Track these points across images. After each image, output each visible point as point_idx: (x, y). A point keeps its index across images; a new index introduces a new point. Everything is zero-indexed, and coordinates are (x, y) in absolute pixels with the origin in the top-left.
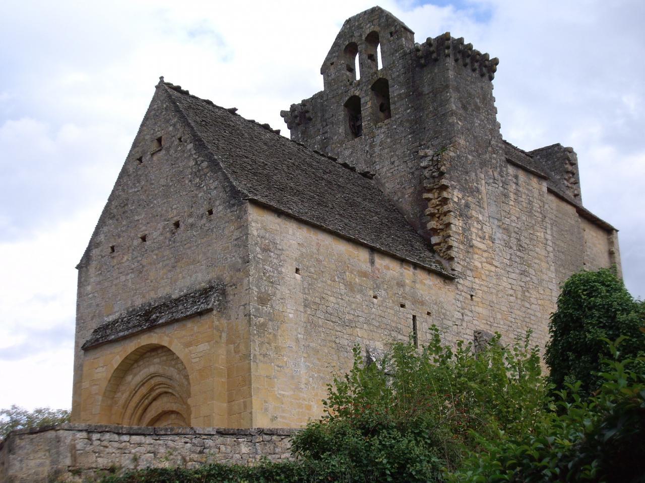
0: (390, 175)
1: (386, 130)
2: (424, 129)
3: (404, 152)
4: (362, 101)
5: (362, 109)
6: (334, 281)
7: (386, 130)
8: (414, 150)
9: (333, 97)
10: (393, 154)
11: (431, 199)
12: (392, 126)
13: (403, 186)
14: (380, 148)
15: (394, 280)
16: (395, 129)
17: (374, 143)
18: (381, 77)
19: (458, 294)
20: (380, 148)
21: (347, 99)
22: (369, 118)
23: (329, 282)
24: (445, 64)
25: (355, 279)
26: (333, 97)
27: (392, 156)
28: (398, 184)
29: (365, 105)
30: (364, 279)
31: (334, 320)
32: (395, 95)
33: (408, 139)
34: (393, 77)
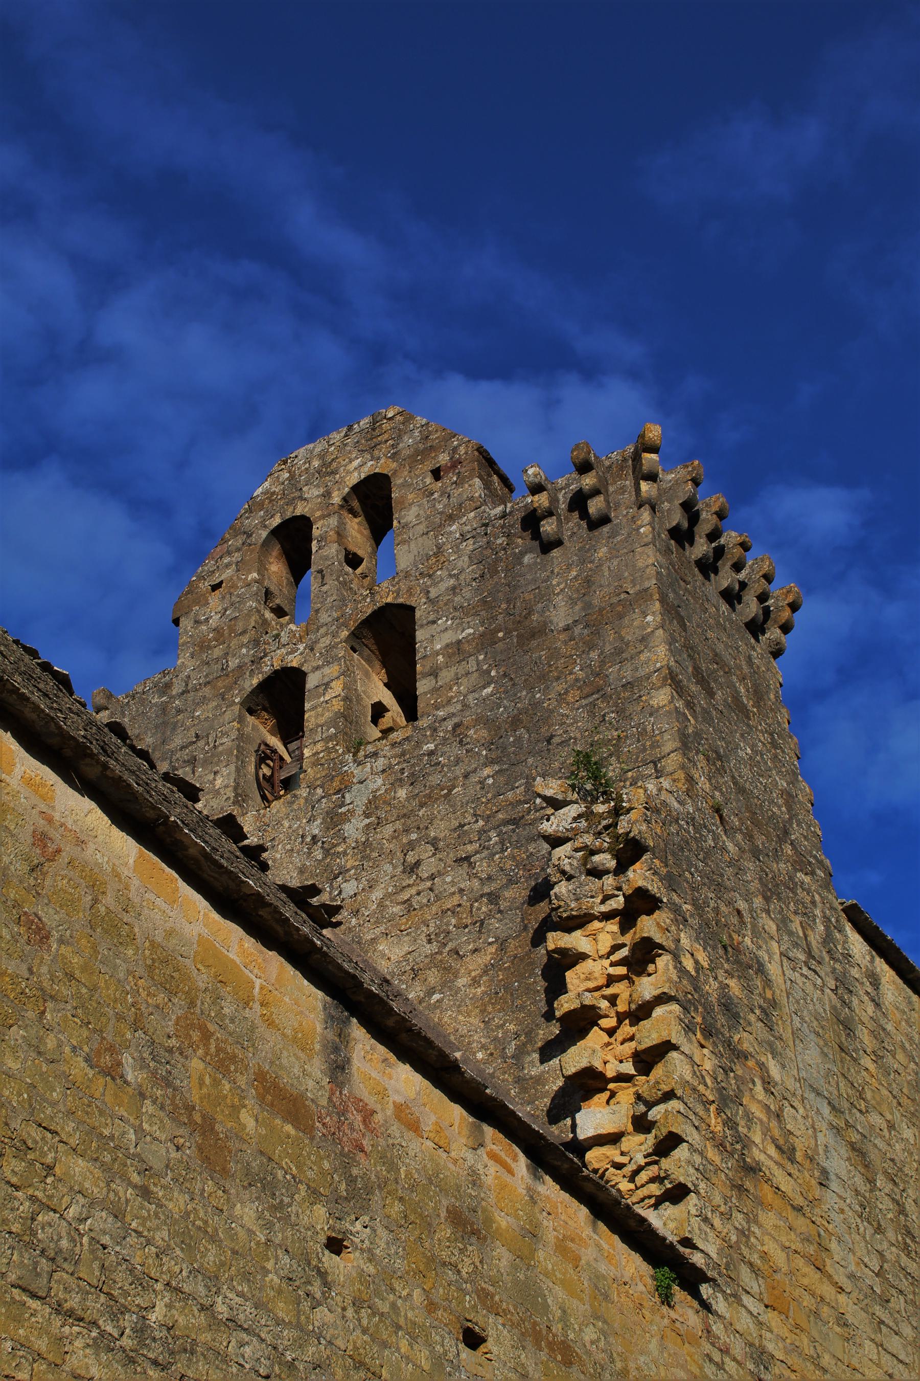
0: (397, 909)
1: (394, 761)
2: (549, 741)
3: (462, 826)
4: (312, 681)
5: (307, 706)
6: (113, 1072)
7: (394, 761)
8: (500, 816)
9: (207, 683)
10: (414, 836)
11: (583, 957)
12: (418, 745)
13: (450, 946)
14: (367, 821)
15: (444, 1191)
16: (431, 753)
17: (343, 810)
18: (389, 600)
19: (711, 1360)
20: (367, 821)
21: (255, 682)
22: (332, 730)
23: (79, 1068)
24: (638, 529)
25: (235, 1110)
26: (207, 683)
27: (411, 846)
28: (430, 941)
29: (321, 690)
30: (289, 1128)
31: (73, 1302)
32: (439, 647)
33: (482, 782)
34: (433, 595)
